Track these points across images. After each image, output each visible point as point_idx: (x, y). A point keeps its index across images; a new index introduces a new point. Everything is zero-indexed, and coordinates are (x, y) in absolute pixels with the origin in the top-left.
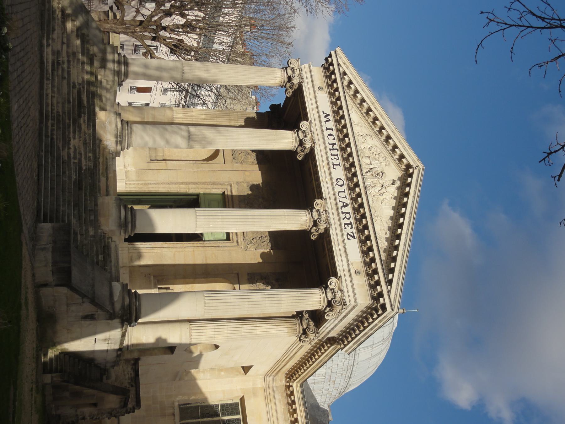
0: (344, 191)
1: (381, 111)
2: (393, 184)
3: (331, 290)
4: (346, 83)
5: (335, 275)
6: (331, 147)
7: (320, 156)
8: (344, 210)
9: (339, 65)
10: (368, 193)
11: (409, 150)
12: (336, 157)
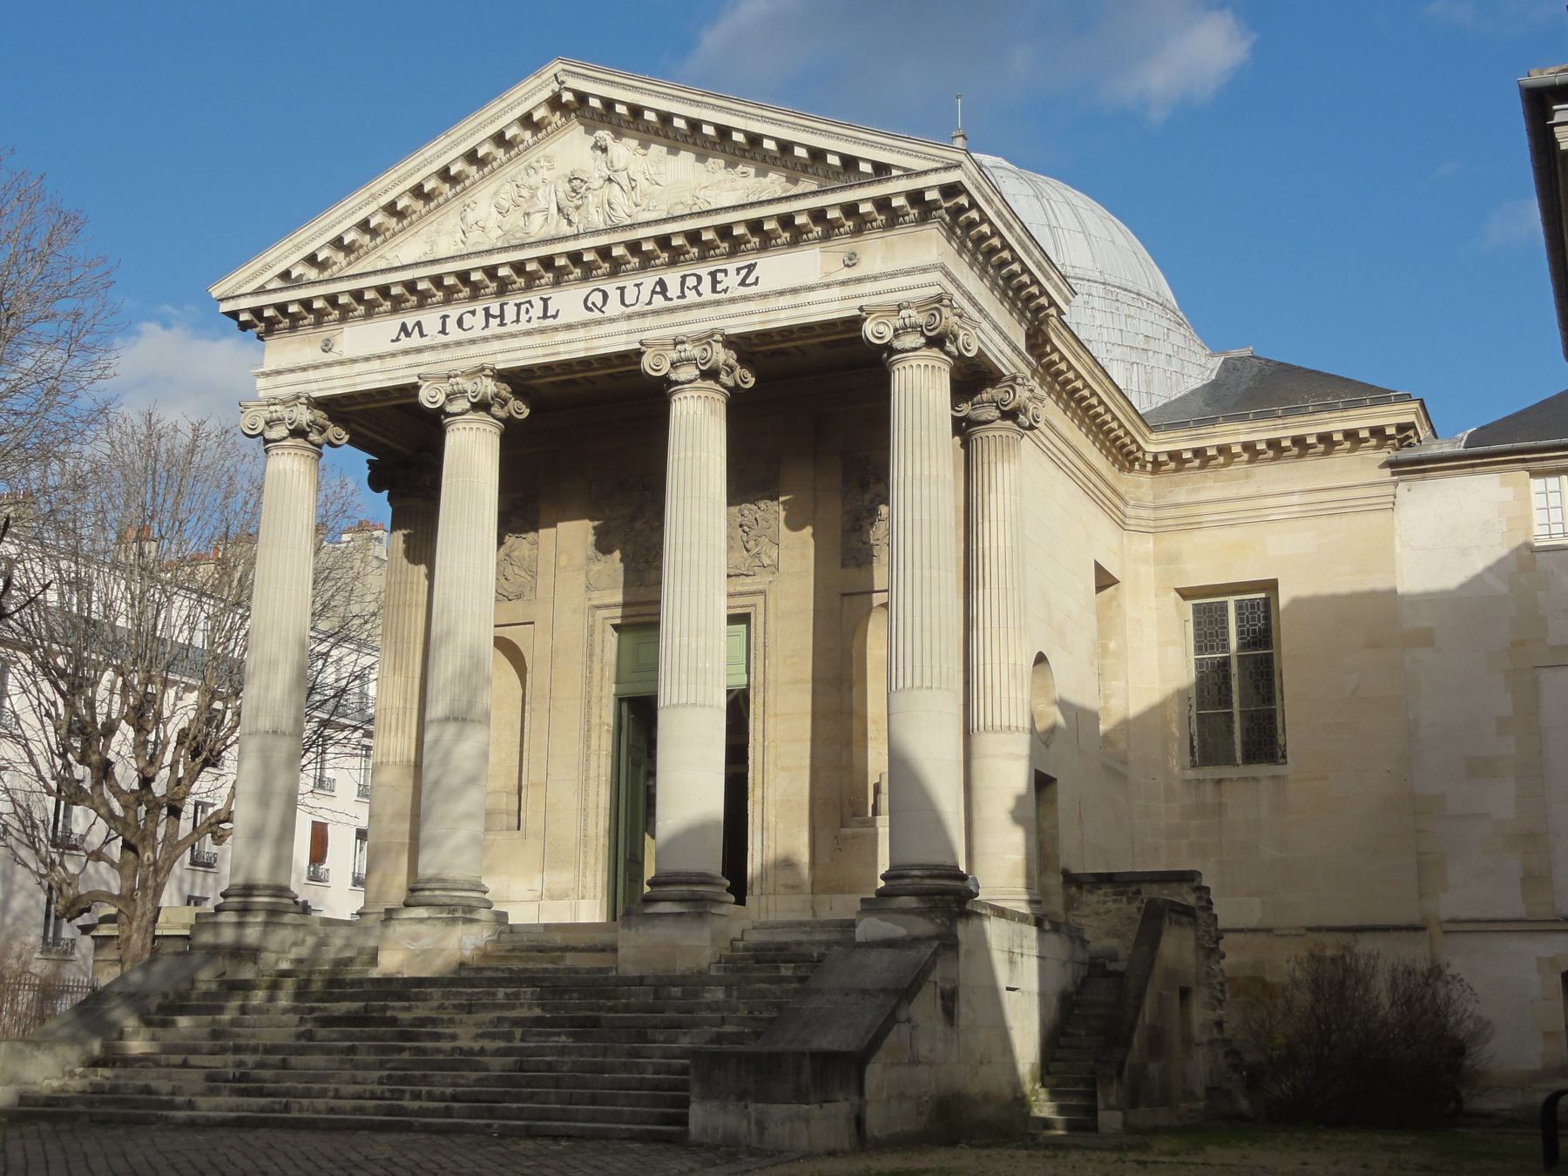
1: (395, 175)
2: (604, 150)
3: (896, 336)
4: (313, 274)
6: (494, 322)
7: (519, 354)
10: (629, 222)
12: (524, 308)
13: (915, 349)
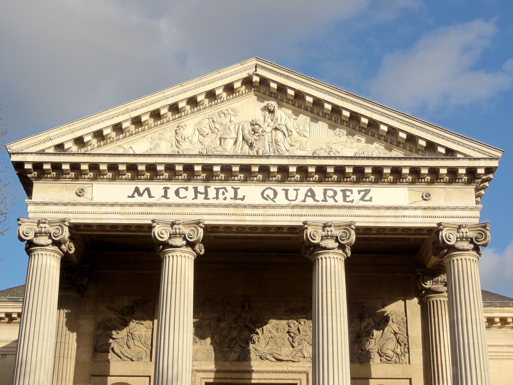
0: (286, 191)
1: (144, 102)
2: (272, 112)
3: (170, 238)
4: (75, 149)
5: (150, 227)
6: (201, 197)
8: (319, 196)
9: (42, 153)
10: (287, 154)
11: (222, 74)
12: (226, 192)
13: (468, 250)
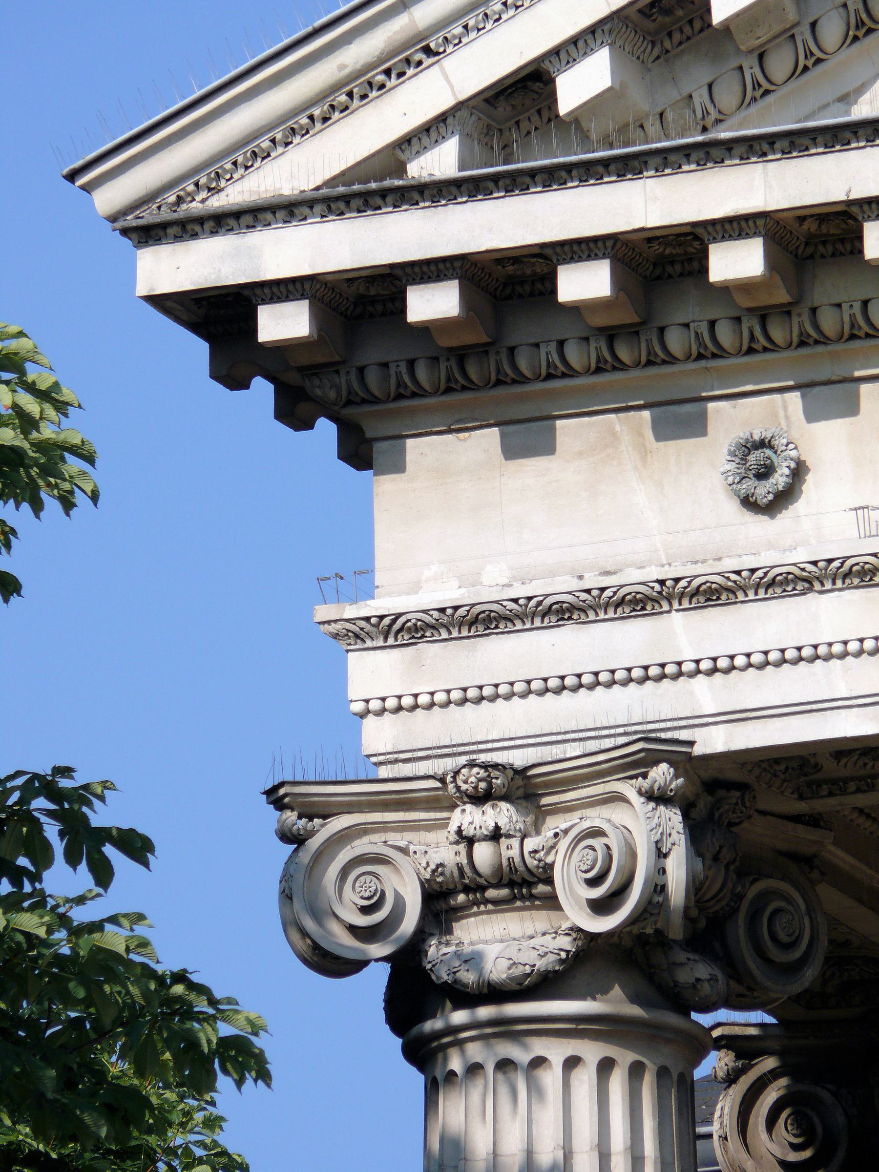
9: (374, 188)
